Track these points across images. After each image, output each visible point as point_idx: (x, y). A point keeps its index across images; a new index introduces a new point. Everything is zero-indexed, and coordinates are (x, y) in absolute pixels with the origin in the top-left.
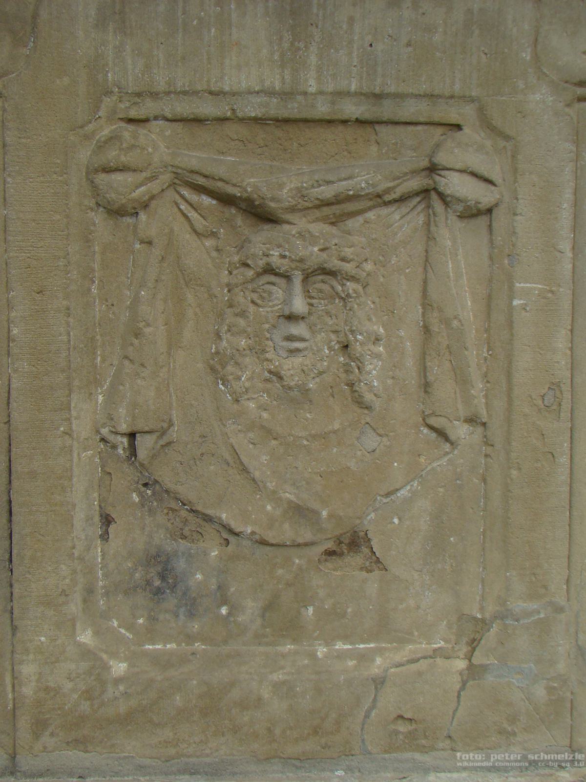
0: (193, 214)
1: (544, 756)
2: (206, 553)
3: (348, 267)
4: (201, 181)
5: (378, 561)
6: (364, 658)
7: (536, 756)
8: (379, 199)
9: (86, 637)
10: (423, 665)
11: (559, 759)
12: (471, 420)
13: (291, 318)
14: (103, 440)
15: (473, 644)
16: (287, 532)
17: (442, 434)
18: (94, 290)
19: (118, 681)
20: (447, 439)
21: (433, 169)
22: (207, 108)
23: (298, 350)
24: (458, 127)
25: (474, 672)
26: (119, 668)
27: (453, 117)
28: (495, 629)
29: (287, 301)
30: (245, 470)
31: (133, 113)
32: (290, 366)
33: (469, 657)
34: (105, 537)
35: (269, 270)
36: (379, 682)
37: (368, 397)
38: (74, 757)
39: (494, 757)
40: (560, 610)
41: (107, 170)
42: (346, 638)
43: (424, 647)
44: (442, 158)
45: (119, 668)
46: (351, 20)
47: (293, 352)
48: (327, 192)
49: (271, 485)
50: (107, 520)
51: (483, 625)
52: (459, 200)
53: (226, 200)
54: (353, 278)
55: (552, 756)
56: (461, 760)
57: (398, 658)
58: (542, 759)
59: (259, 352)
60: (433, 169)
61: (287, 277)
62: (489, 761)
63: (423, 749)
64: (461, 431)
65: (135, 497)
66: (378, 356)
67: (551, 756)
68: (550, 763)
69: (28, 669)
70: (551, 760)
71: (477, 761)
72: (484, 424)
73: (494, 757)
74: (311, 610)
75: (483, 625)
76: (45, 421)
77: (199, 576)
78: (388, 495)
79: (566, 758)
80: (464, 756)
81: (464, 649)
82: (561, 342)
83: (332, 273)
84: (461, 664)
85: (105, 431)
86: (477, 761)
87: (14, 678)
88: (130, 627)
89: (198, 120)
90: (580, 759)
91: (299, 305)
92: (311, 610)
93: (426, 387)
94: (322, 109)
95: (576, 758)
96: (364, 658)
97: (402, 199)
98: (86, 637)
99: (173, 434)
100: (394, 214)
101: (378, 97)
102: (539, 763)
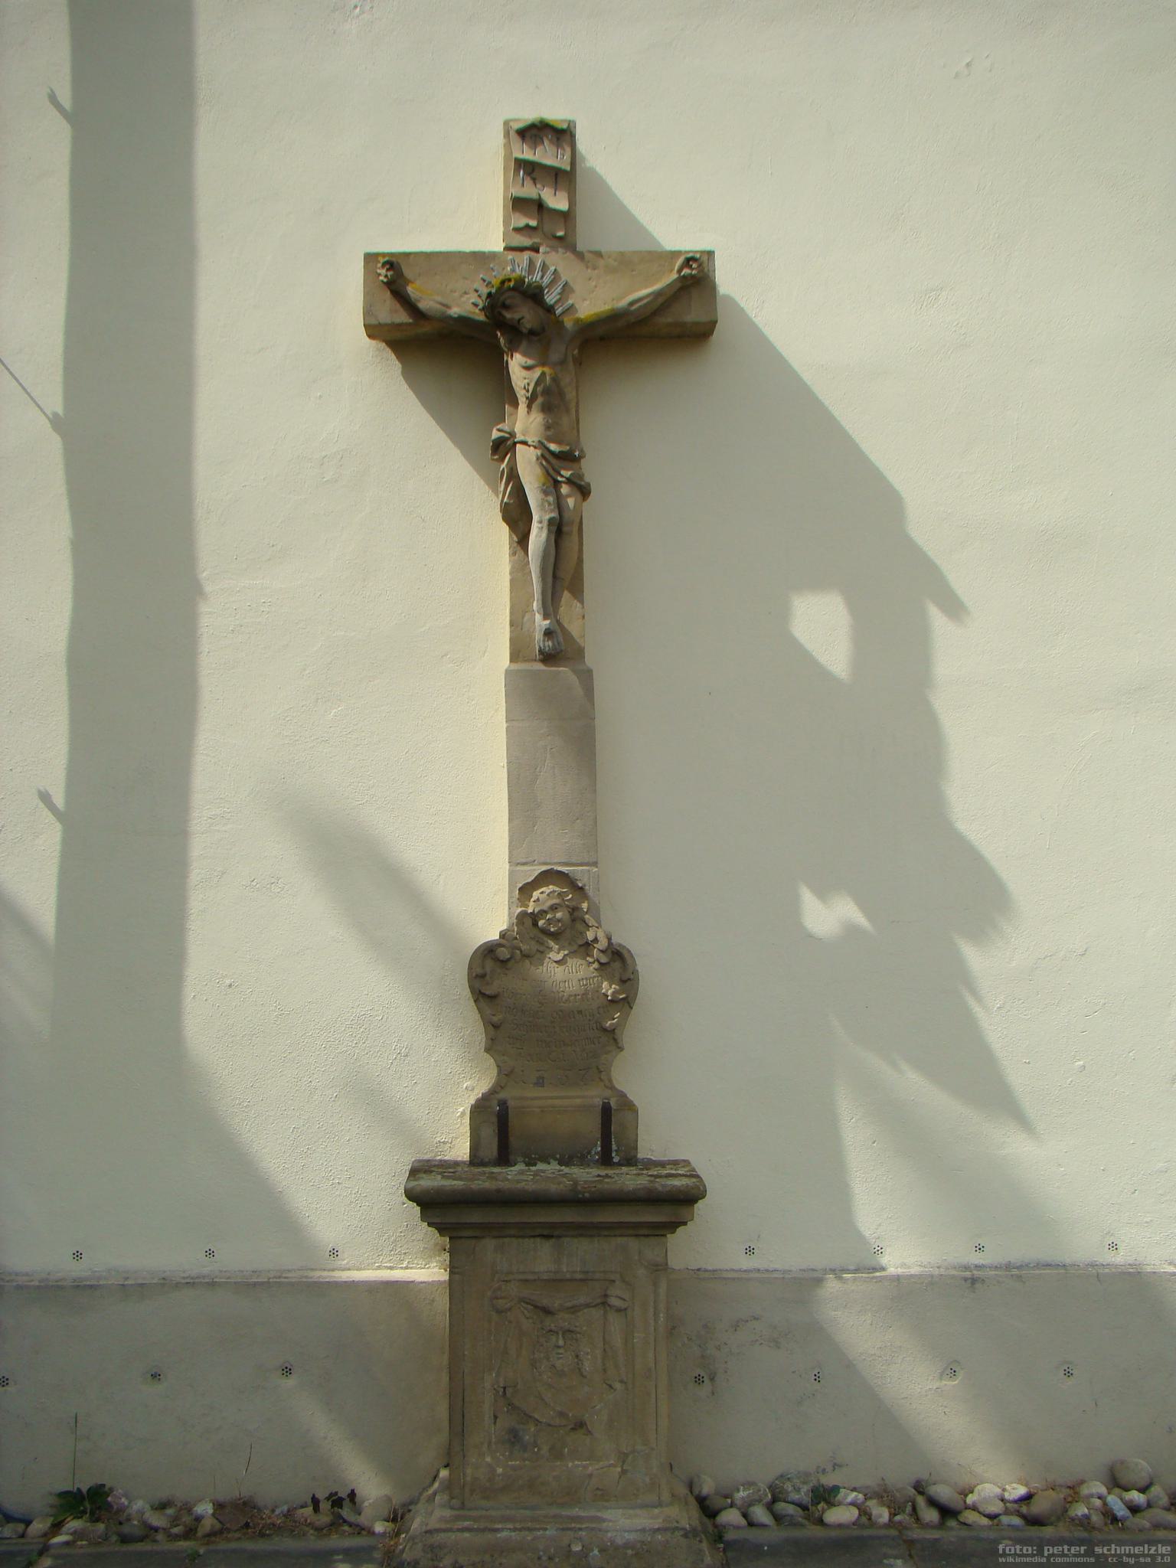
0: (526, 1312)
1: (1116, 1549)
2: (530, 1429)
3: (578, 1329)
4: (528, 1301)
5: (590, 1432)
6: (585, 1467)
7: (1105, 1549)
8: (588, 1306)
9: (488, 1459)
10: (605, 1469)
11: (1136, 1552)
12: (621, 1381)
13: (559, 1347)
14: (495, 1389)
15: (624, 1462)
16: (557, 1421)
17: (610, 1386)
18: (492, 1338)
19: (499, 1475)
20: (612, 1388)
21: (606, 1296)
22: (531, 1277)
23: (561, 1358)
24: (614, 1281)
25: (624, 1472)
26: (500, 1470)
27: (613, 1278)
28: (630, 1457)
29: (557, 1341)
30: (543, 1400)
31: (506, 1279)
32: (559, 1364)
33: (622, 1467)
34: (495, 1423)
35: (551, 1331)
36: (590, 1476)
37: (585, 1373)
38: (483, 1503)
39: (1048, 1550)
40: (653, 1449)
41: (497, 1298)
42: (579, 1460)
43: (606, 1463)
44: (609, 1292)
45: (500, 1470)
46: (577, 1248)
47: (559, 1358)
48: (569, 1304)
49: (552, 1405)
50: (496, 1417)
51: (626, 1455)
52: (615, 1306)
53: (536, 1307)
54: (580, 1333)
55: (1127, 1548)
56: (1004, 1555)
57: (597, 1467)
58: (1113, 1552)
59: (548, 1359)
60: (606, 1296)
61: (557, 1333)
62: (1043, 1556)
63: (607, 1501)
64: (618, 1386)
65: (506, 1409)
66: (588, 1359)
67: (1125, 1549)
68: (1124, 1558)
69: (469, 1471)
70: (1125, 1554)
71: (1027, 1556)
72: (625, 1383)
73: (1048, 1550)
74: (566, 1450)
75: (626, 1455)
76: (472, 1074)
77: (527, 1437)
78: (592, 1408)
79: (1146, 1552)
80: (1008, 1548)
81: (621, 1464)
82: (651, 1355)
83: (572, 1332)
84: (619, 1469)
85: (496, 1387)
86: (1027, 1556)
87: (463, 1474)
88: (503, 1455)
89: (526, 1281)
90: (1164, 1552)
91: (561, 1342)
92: (566, 1450)
93: (605, 1370)
94: (568, 1276)
95: (1160, 1553)
96: (585, 1467)
97: (595, 1306)
98: (488, 1459)
99: (519, 1387)
100: (593, 1311)
101: (588, 1272)
102: (1110, 1559)
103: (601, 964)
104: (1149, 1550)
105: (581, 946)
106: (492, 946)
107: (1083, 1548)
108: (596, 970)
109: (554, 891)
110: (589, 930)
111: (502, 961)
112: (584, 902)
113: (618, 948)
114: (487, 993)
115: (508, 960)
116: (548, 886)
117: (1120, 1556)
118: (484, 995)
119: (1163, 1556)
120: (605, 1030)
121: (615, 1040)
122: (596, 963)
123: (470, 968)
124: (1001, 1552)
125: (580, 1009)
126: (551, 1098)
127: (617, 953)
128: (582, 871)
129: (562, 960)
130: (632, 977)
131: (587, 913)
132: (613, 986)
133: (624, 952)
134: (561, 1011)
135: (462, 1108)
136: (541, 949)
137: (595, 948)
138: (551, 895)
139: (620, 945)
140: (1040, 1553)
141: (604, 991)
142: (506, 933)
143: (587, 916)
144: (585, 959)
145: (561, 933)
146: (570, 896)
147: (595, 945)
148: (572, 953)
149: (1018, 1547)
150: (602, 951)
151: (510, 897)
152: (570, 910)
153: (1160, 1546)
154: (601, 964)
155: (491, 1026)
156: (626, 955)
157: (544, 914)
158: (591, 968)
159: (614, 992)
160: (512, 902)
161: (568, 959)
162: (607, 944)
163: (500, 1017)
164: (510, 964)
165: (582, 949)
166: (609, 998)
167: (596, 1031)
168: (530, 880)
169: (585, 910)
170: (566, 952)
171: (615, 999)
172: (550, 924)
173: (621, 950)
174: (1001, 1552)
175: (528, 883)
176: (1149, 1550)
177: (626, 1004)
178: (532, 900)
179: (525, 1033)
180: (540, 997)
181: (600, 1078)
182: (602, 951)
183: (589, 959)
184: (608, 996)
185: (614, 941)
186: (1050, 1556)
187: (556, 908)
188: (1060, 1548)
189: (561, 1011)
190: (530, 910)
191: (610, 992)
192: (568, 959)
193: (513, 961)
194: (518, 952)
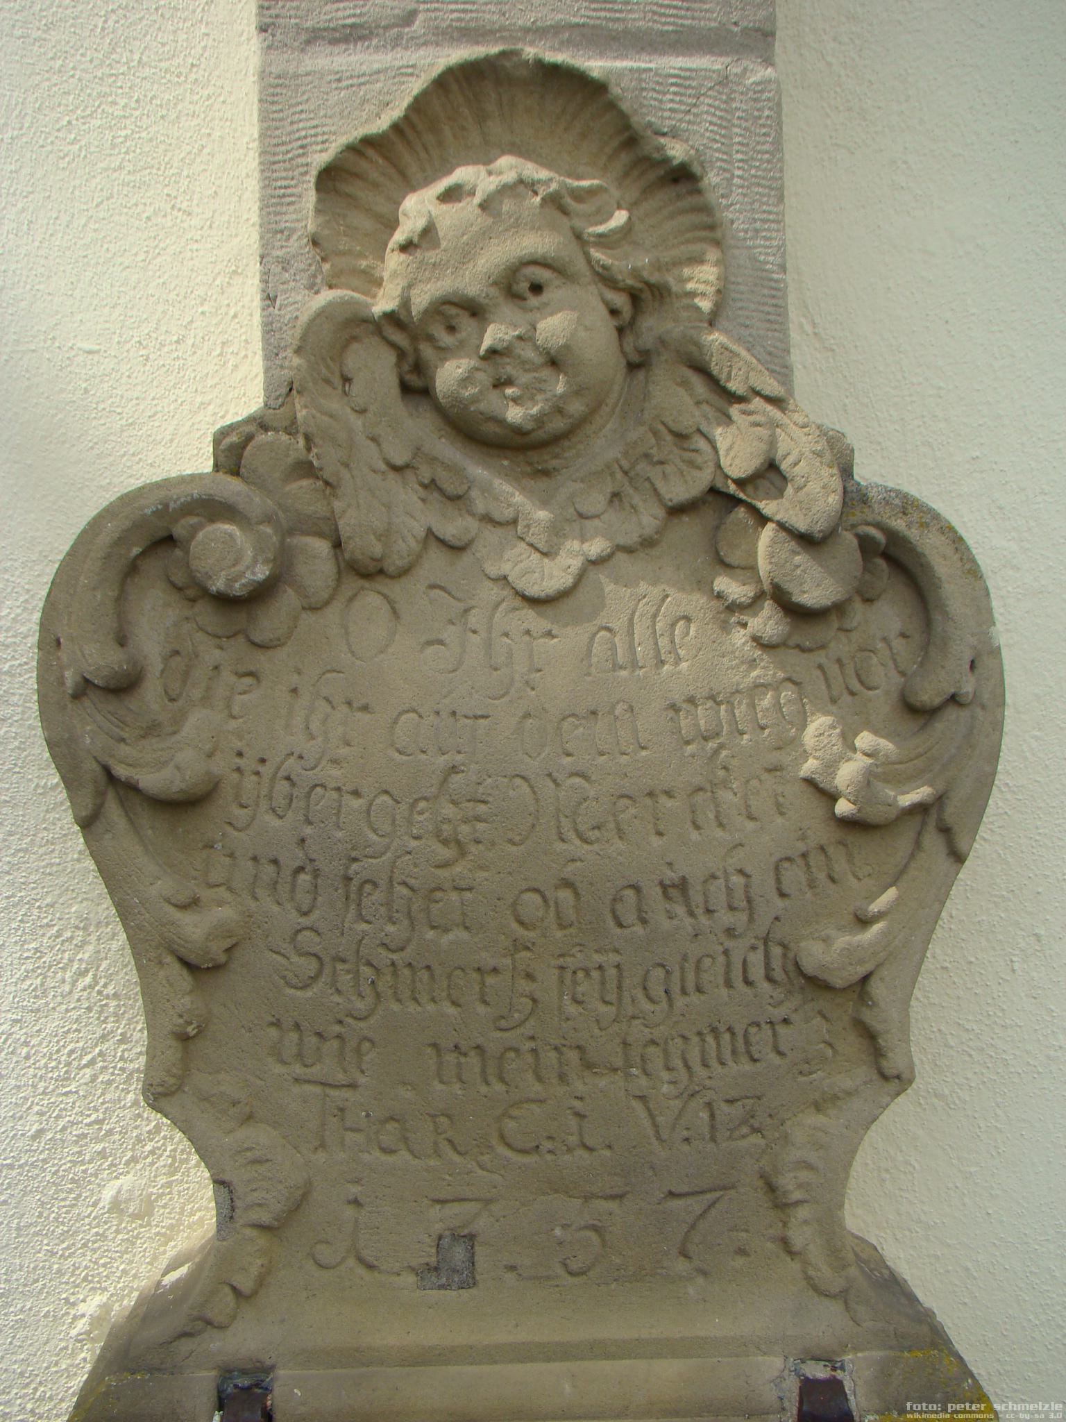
70: (1021, 1411)
86: (932, 1412)
103: (797, 613)
104: (1043, 1407)
105: (677, 511)
106: (163, 511)
107: (983, 1405)
108: (766, 646)
109: (524, 185)
110: (729, 420)
111: (225, 601)
112: (698, 260)
113: (899, 524)
114: (150, 780)
115: (261, 594)
116: (488, 161)
117: (1016, 1413)
118: (127, 790)
119: (1055, 1412)
120: (816, 984)
121: (869, 1036)
122: (768, 606)
123: (50, 642)
124: (908, 1409)
125: (670, 876)
126: (492, 1354)
127: (886, 556)
128: (684, 79)
129: (563, 595)
130: (968, 687)
131: (712, 321)
132: (865, 740)
133: (930, 545)
134: (567, 884)
135: (98, 1299)
136: (453, 527)
137: (763, 520)
138: (507, 206)
139: (908, 505)
140: (945, 1410)
141: (810, 766)
142: (249, 438)
143: (715, 338)
144: (703, 584)
145: (556, 440)
146: (620, 218)
147: (767, 507)
148: (629, 550)
149: (924, 1405)
150: (806, 540)
151: (272, 231)
152: (620, 300)
153: (1052, 1403)
154: (797, 613)
155: (177, 966)
156: (942, 566)
157: (467, 325)
158: (739, 637)
159: (869, 779)
160: (285, 264)
161: (609, 588)
162: (834, 500)
163: (226, 913)
164: (270, 621)
165: (690, 529)
166: (843, 807)
167: (765, 986)
168: (381, 124)
169: (705, 305)
170: (596, 547)
171: (875, 814)
172: (500, 384)
173: (913, 534)
174: (908, 1409)
175: (368, 142)
176: (1043, 1407)
177: (933, 842)
178: (399, 236)
179: (361, 1006)
180: (448, 810)
181: (785, 1243)
182: (806, 540)
183: (734, 588)
184: (832, 797)
185: (864, 473)
186: (952, 1413)
187: (537, 288)
188: (963, 1406)
189: (567, 884)
190: (383, 303)
191: (847, 774)
192: (609, 588)
193: (288, 599)
194: (322, 547)
